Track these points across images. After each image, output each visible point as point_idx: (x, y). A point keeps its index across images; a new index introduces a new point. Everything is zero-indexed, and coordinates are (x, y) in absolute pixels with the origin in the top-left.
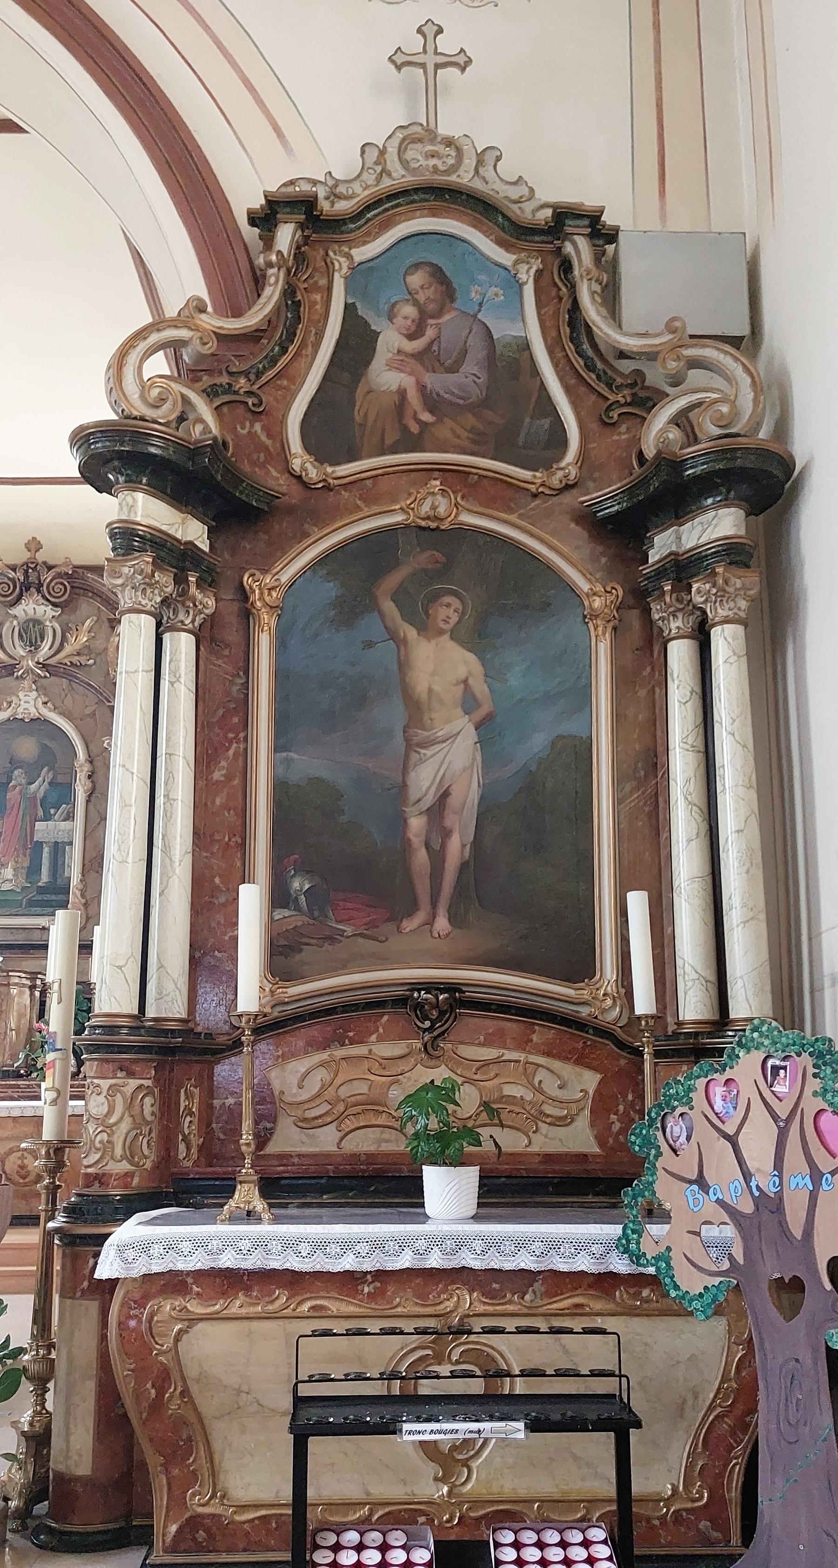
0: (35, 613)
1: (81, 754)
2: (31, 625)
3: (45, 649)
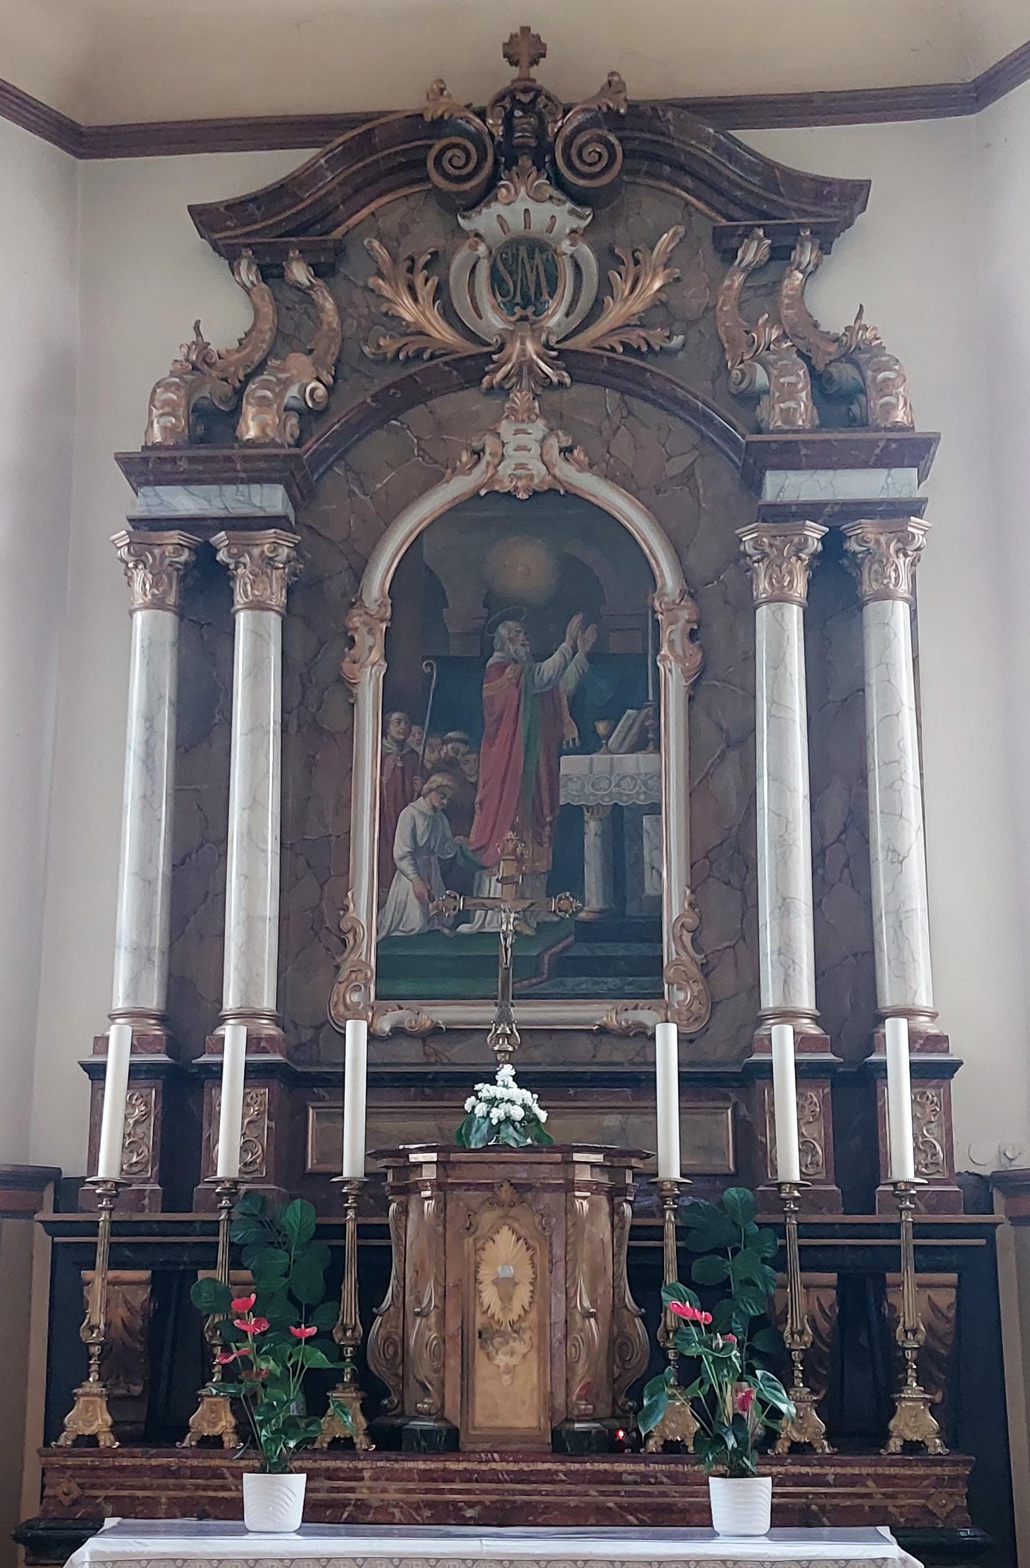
0: (527, 225)
2: (523, 253)
3: (555, 317)
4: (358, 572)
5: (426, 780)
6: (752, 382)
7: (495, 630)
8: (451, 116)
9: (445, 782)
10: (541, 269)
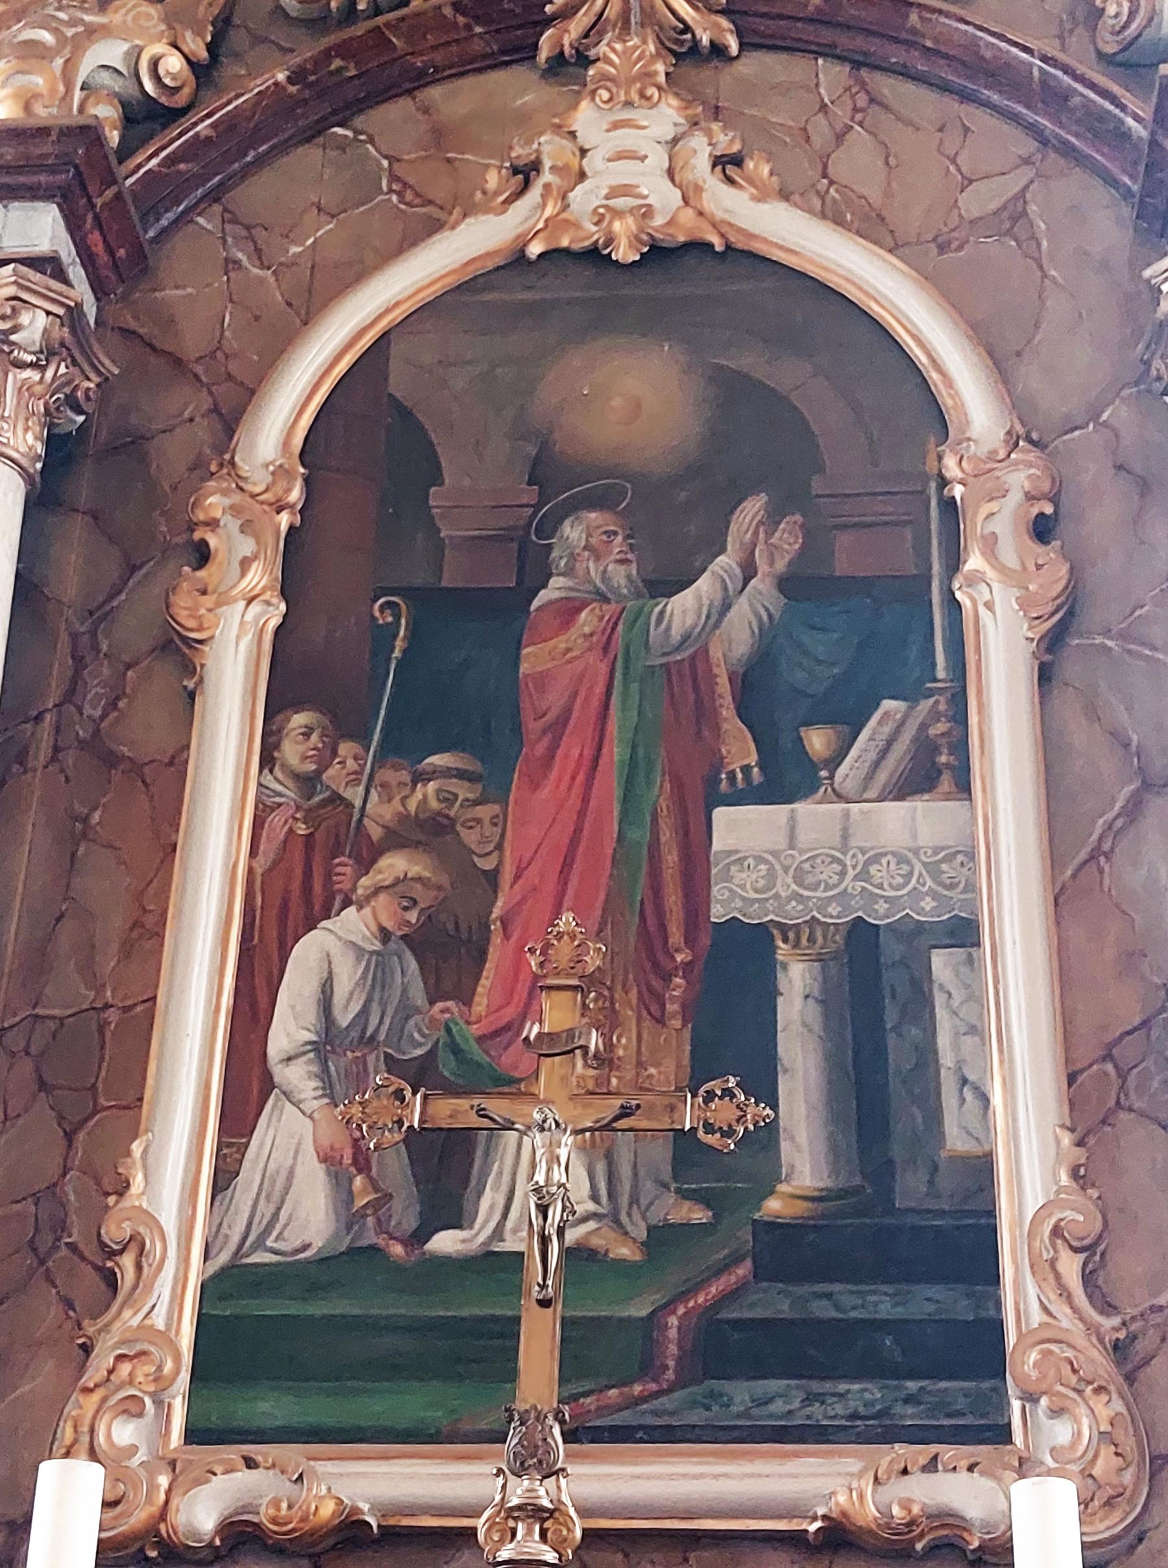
1: (975, 403)
4: (229, 420)
5: (366, 864)
7: (554, 530)
9: (415, 870)
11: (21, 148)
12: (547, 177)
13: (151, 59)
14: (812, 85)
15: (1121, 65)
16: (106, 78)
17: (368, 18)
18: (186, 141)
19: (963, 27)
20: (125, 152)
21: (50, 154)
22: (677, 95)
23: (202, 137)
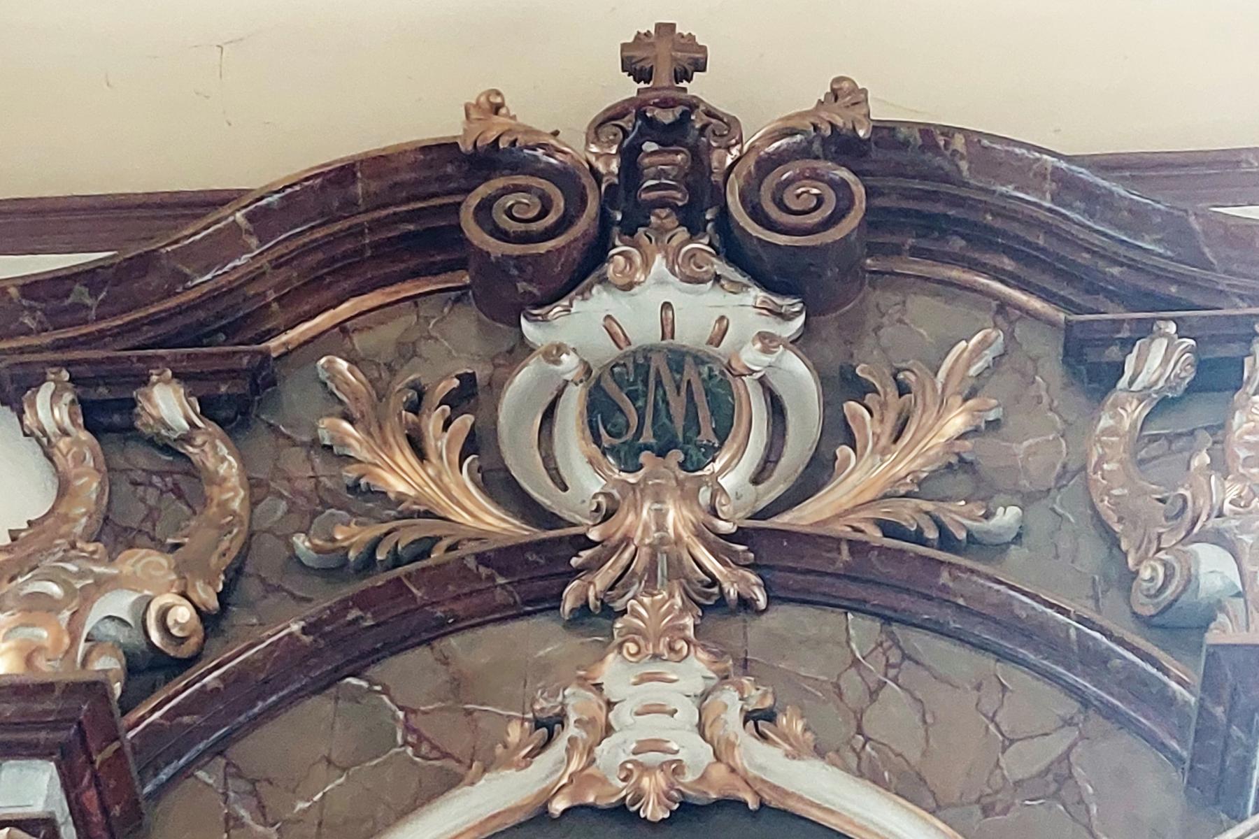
0: (668, 329)
6: (1190, 580)
8: (513, 143)
10: (697, 387)
11: (22, 704)
12: (572, 730)
13: (161, 607)
14: (844, 639)
15: (1162, 627)
16: (111, 629)
17: (388, 569)
18: (191, 694)
19: (997, 587)
20: (127, 705)
21: (53, 711)
22: (704, 647)
23: (209, 688)
